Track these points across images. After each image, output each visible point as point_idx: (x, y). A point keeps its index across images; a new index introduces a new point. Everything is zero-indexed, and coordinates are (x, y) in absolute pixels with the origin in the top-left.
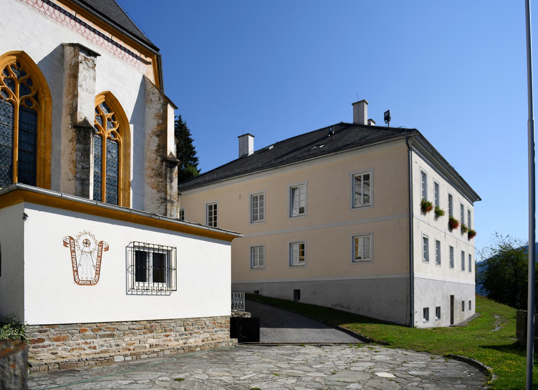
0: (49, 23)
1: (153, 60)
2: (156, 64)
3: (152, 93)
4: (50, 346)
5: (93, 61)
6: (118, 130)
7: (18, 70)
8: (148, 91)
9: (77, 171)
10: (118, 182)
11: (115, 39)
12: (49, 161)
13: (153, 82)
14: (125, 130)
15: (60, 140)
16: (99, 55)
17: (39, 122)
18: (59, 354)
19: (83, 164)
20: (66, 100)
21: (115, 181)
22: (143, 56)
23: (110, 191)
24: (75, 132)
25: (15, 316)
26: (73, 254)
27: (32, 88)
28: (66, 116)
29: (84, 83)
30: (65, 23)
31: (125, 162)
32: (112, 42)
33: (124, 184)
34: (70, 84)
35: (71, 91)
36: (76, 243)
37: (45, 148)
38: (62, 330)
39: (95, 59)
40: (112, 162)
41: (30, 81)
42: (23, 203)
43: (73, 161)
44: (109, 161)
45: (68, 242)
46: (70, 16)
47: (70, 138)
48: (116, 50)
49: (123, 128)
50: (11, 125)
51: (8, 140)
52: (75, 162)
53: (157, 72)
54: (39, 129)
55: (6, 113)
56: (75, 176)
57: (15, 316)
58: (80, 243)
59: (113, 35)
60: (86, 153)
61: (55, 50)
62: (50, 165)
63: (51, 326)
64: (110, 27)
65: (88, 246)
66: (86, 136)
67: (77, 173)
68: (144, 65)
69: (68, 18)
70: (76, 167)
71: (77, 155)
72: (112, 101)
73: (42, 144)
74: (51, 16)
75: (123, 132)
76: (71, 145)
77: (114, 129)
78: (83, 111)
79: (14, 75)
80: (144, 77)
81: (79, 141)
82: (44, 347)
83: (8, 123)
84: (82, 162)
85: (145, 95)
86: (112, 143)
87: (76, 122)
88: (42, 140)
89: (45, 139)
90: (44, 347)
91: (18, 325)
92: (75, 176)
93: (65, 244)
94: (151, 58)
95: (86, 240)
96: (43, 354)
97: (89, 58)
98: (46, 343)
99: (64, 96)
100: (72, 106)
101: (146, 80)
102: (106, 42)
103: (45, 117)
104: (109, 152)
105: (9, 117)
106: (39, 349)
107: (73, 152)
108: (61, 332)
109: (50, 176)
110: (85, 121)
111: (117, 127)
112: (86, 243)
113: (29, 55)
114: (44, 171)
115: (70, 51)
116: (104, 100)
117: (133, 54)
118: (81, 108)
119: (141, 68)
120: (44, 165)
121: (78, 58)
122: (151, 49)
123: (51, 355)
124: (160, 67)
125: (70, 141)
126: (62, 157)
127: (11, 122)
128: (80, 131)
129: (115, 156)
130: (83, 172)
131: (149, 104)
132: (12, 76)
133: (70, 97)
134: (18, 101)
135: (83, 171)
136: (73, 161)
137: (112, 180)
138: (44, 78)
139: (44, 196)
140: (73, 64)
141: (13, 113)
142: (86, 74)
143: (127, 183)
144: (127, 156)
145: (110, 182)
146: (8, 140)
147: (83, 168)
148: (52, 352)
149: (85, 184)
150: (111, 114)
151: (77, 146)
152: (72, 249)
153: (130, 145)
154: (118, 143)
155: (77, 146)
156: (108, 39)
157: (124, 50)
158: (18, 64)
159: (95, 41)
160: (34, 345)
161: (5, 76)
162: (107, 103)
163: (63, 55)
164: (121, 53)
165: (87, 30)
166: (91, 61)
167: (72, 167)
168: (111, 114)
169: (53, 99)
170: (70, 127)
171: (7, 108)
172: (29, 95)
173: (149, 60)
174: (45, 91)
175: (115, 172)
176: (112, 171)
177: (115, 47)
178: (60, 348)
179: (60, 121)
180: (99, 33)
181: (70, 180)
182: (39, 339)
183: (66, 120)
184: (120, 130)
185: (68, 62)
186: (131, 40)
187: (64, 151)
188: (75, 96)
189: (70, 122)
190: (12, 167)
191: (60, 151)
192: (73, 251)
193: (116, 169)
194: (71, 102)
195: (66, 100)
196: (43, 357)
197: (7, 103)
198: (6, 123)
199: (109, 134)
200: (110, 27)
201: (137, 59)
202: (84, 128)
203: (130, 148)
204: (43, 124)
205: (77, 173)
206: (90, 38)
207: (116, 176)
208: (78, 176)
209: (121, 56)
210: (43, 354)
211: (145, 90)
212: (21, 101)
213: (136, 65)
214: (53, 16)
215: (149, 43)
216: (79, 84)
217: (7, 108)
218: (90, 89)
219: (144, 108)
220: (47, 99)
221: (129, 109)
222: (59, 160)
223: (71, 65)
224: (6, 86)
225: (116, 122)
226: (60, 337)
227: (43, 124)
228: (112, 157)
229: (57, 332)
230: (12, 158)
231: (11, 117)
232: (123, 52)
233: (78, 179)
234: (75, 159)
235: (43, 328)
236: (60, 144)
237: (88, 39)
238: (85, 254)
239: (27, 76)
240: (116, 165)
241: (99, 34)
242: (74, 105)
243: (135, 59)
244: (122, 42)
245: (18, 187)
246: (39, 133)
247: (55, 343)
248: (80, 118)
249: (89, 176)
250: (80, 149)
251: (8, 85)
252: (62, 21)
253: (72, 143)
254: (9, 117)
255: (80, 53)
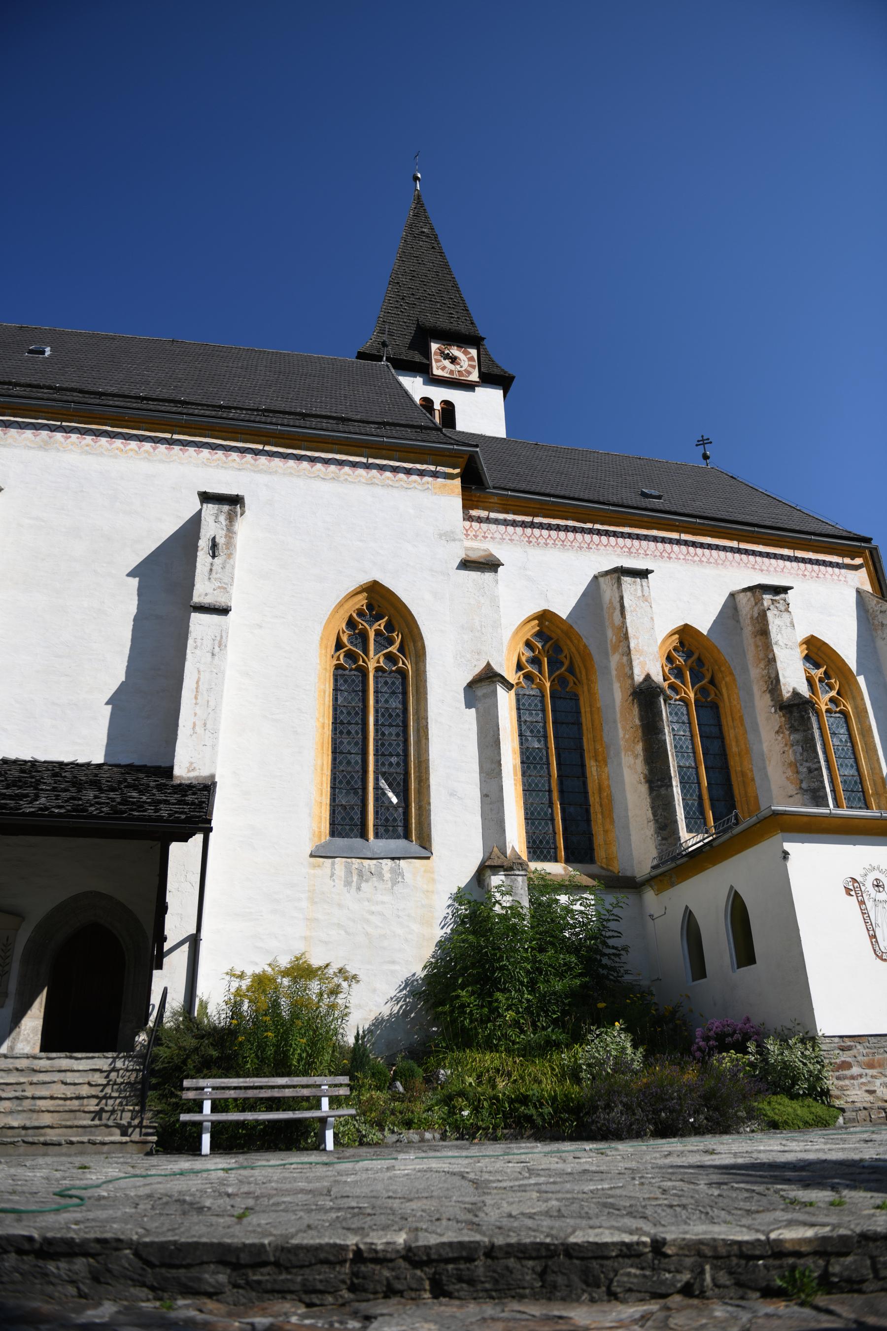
0: (709, 572)
1: (865, 559)
2: (870, 563)
3: (881, 612)
4: (861, 1076)
5: (785, 600)
6: (838, 693)
7: (683, 652)
8: (871, 611)
9: (802, 777)
10: (861, 783)
11: (800, 554)
12: (750, 774)
13: (870, 590)
14: (851, 690)
15: (759, 736)
16: (791, 588)
17: (723, 717)
18: (879, 1093)
19: (808, 764)
20: (755, 672)
21: (856, 782)
22: (847, 561)
23: (852, 802)
24: (784, 716)
25: (798, 1024)
26: (863, 907)
27: (704, 670)
28: (761, 696)
29: (779, 637)
30: (728, 563)
31: (865, 744)
32: (796, 559)
33: (875, 784)
34: (757, 646)
35: (762, 655)
36: (863, 888)
37: (739, 755)
38: (875, 1047)
39: (786, 596)
40: (843, 749)
41: (700, 661)
42: (780, 836)
43: (790, 764)
44: (838, 749)
45: (851, 887)
46: (732, 550)
47: (777, 728)
48: (806, 569)
49: (847, 687)
50: (688, 734)
51: (689, 757)
52: (794, 765)
53: (873, 574)
54: (725, 729)
55: (680, 718)
56: (801, 788)
57: (798, 1024)
58: (869, 886)
59: (794, 548)
60: (808, 745)
61: (725, 606)
62: (753, 780)
63: (857, 1039)
64: (788, 540)
65: (881, 889)
66: (802, 717)
67: (801, 781)
68: (854, 572)
69: (729, 555)
70: (798, 772)
71: (795, 753)
72: (819, 649)
73: (735, 749)
74: (709, 562)
75: (849, 693)
76: (780, 738)
77: (833, 693)
78: (787, 679)
79: (680, 660)
80: (859, 592)
81: (793, 729)
82: (853, 1078)
83: (684, 731)
84: (807, 761)
85: (868, 619)
86: (835, 717)
87: (782, 700)
88: (734, 744)
89: (737, 741)
90: (853, 1078)
91: (810, 1038)
92: (801, 788)
93: (848, 891)
94: (860, 557)
95: (876, 879)
96: (854, 1092)
97: (777, 598)
98: (855, 1070)
99: (750, 667)
100: (769, 678)
101: (864, 595)
102: (788, 563)
103: (731, 706)
104: (833, 734)
105: (683, 723)
106: (847, 1082)
107: (786, 749)
108: (873, 1051)
109: (756, 797)
110: (796, 694)
111: (837, 688)
112: (877, 886)
113: (694, 625)
114: (746, 792)
115: (746, 599)
116: (806, 652)
117: (831, 564)
118: (784, 677)
119: (849, 580)
120: (744, 782)
121: (762, 604)
122: (858, 544)
123: (867, 1095)
124: (878, 565)
125: (777, 732)
126: (767, 762)
127: (688, 729)
128: (791, 712)
129: (844, 738)
130: (812, 778)
131: (879, 632)
132: (400, 665)
133: (762, 665)
134: (692, 695)
135: (812, 775)
136: (790, 764)
137: (850, 782)
138: (718, 650)
139: (805, 819)
140: (756, 615)
141: (688, 714)
142: (779, 623)
143: (879, 781)
144: (866, 732)
145: (849, 786)
146: (689, 757)
147: (810, 771)
148: (867, 1088)
149: (820, 797)
150: (822, 670)
151: (792, 738)
152: (860, 898)
153: (867, 712)
154: (845, 714)
155: (792, 738)
156: (789, 559)
157: (816, 564)
158: (681, 643)
159: (772, 569)
160: (837, 1074)
161: (669, 666)
162: (813, 655)
163: (735, 609)
164: (813, 570)
165: (759, 559)
166: (781, 602)
167: (791, 774)
168: (822, 670)
169: (737, 677)
170: (773, 710)
171: (679, 710)
172: (703, 682)
173: (858, 561)
174: (723, 669)
175: (852, 766)
176: (847, 765)
177: (802, 565)
178: (878, 1082)
179: (753, 707)
180: (775, 554)
181: (791, 796)
182: (843, 1062)
183: (762, 704)
184: (843, 692)
185: (746, 615)
186: (823, 545)
187: (770, 751)
188: (771, 661)
189: (771, 703)
190: (700, 797)
191: (763, 754)
192: (862, 903)
193: (852, 761)
194: (766, 671)
195: (755, 672)
196: (855, 1098)
197: (677, 703)
198: (682, 733)
199: (826, 705)
200: (788, 540)
201: (840, 568)
202: (798, 705)
203: (868, 717)
204: (729, 718)
205: (801, 781)
206: (765, 568)
207: (856, 774)
208: (804, 785)
209: (814, 574)
210: (854, 1092)
211: (867, 611)
212: (695, 695)
213: (841, 578)
214: (711, 560)
215: (852, 535)
216: (773, 641)
217: (679, 710)
218: (790, 644)
219: (873, 641)
220: (727, 679)
221: (849, 653)
222: (765, 768)
223: (752, 618)
224: (673, 680)
225: (833, 681)
226: (874, 1060)
227: (729, 718)
228: (841, 741)
229: (868, 1050)
230: (699, 783)
231: (686, 721)
232: (816, 567)
233: (806, 791)
234: (793, 759)
235: (848, 1042)
236: (760, 742)
237: (762, 571)
238: (880, 905)
239: (695, 657)
240: (358, 719)
241: (775, 556)
242: (773, 676)
243: (836, 570)
244: (761, 546)
245: (774, 811)
246: (726, 734)
247: (867, 1071)
248: (786, 693)
249: (822, 782)
250: (798, 742)
251: (675, 678)
252: (724, 561)
253: (782, 735)
254: (683, 723)
255: (764, 596)
